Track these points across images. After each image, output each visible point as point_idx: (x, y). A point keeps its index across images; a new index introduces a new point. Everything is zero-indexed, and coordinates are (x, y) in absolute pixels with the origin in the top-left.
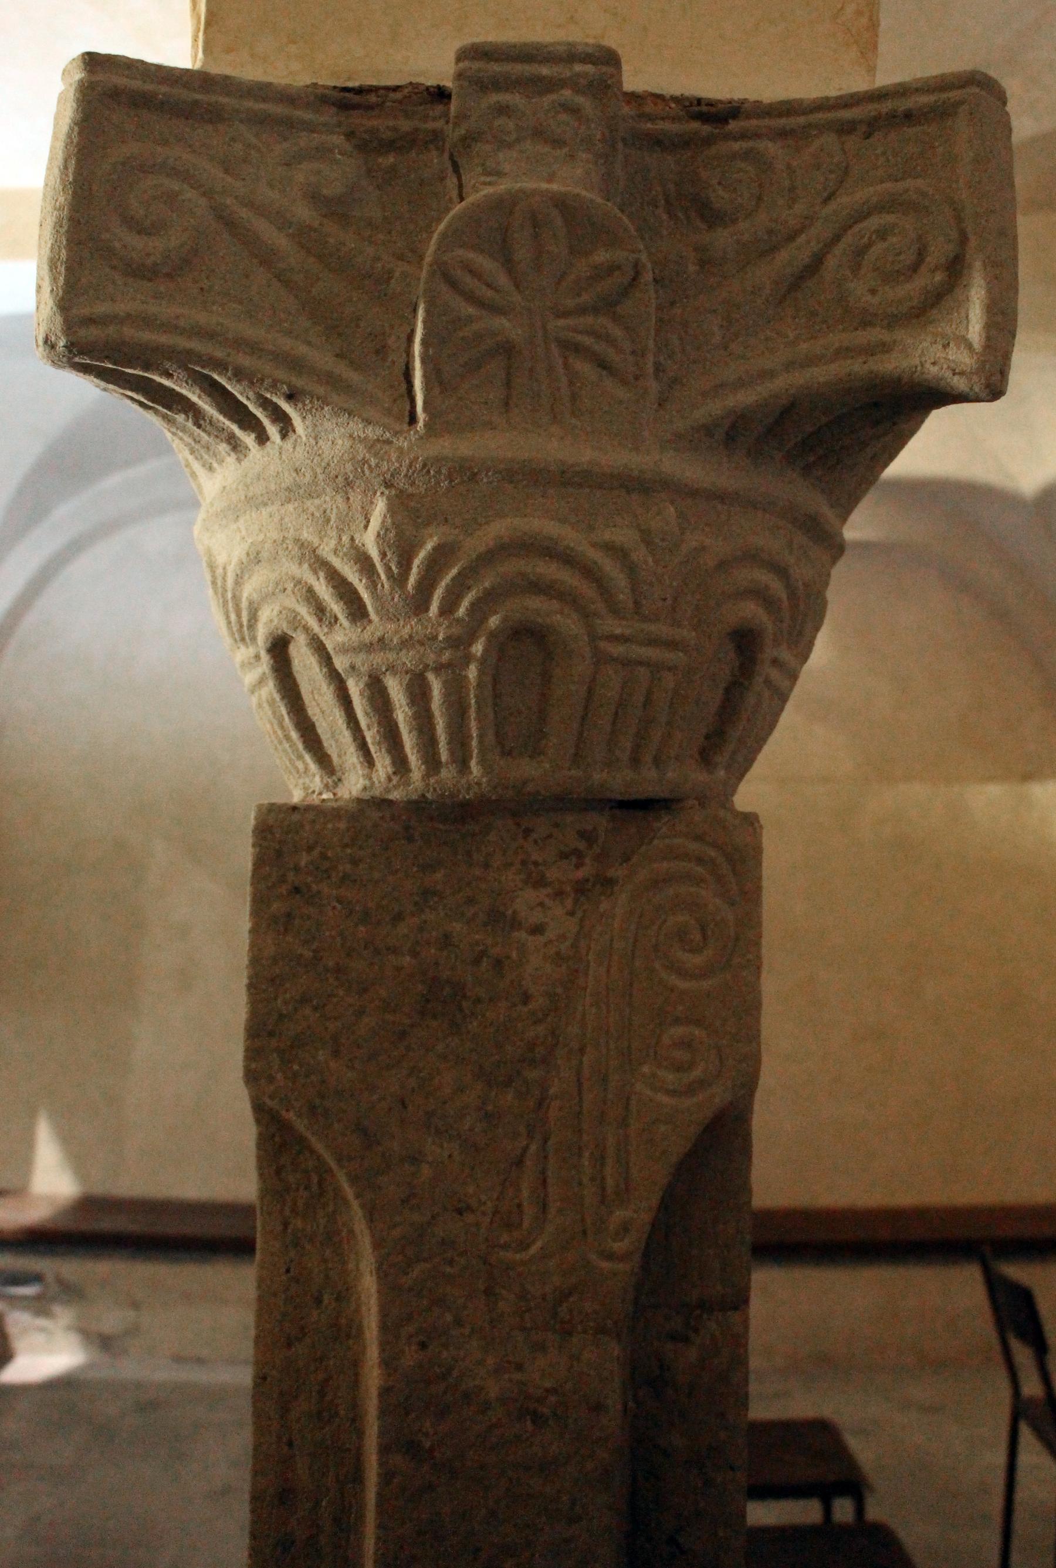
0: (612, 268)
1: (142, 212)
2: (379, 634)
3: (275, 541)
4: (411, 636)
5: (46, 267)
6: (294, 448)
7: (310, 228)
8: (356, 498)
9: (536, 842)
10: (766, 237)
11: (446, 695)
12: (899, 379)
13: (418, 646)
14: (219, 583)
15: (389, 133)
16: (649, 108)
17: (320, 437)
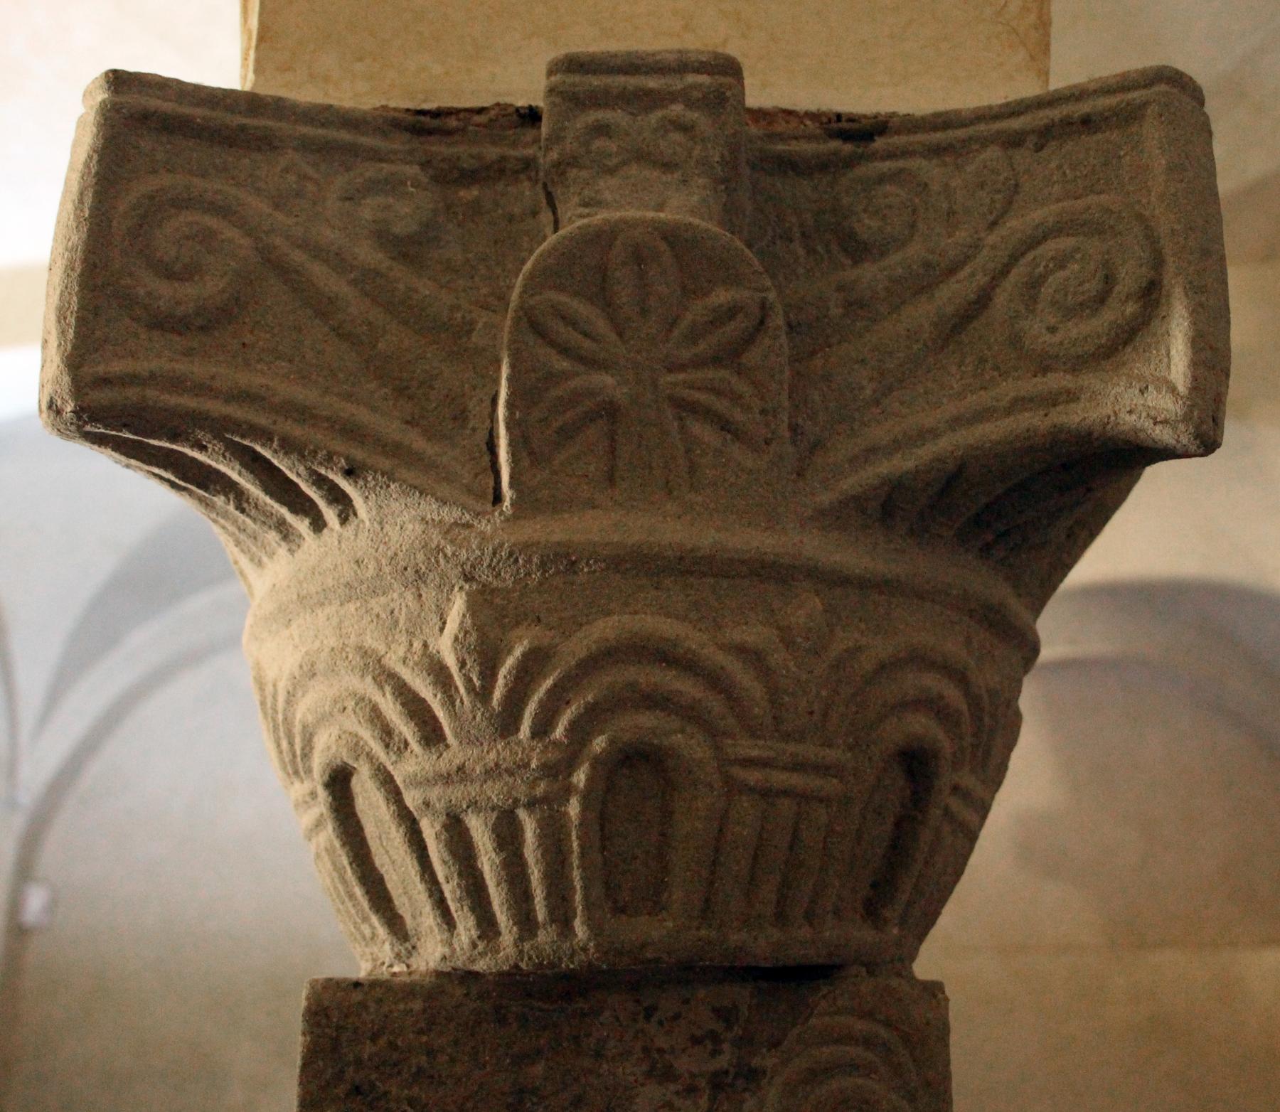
0: (732, 311)
1: (173, 253)
2: (457, 762)
3: (333, 649)
4: (497, 765)
5: (53, 317)
6: (356, 535)
7: (378, 273)
8: (429, 594)
9: (661, 1023)
10: (921, 271)
11: (542, 837)
12: (1090, 434)
13: (506, 776)
14: (269, 701)
15: (472, 161)
16: (781, 127)
17: (386, 522)
